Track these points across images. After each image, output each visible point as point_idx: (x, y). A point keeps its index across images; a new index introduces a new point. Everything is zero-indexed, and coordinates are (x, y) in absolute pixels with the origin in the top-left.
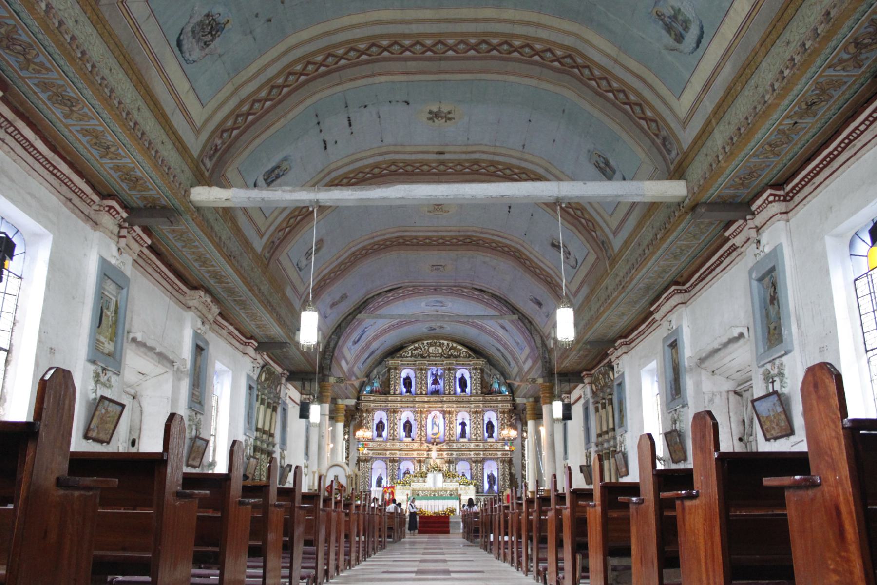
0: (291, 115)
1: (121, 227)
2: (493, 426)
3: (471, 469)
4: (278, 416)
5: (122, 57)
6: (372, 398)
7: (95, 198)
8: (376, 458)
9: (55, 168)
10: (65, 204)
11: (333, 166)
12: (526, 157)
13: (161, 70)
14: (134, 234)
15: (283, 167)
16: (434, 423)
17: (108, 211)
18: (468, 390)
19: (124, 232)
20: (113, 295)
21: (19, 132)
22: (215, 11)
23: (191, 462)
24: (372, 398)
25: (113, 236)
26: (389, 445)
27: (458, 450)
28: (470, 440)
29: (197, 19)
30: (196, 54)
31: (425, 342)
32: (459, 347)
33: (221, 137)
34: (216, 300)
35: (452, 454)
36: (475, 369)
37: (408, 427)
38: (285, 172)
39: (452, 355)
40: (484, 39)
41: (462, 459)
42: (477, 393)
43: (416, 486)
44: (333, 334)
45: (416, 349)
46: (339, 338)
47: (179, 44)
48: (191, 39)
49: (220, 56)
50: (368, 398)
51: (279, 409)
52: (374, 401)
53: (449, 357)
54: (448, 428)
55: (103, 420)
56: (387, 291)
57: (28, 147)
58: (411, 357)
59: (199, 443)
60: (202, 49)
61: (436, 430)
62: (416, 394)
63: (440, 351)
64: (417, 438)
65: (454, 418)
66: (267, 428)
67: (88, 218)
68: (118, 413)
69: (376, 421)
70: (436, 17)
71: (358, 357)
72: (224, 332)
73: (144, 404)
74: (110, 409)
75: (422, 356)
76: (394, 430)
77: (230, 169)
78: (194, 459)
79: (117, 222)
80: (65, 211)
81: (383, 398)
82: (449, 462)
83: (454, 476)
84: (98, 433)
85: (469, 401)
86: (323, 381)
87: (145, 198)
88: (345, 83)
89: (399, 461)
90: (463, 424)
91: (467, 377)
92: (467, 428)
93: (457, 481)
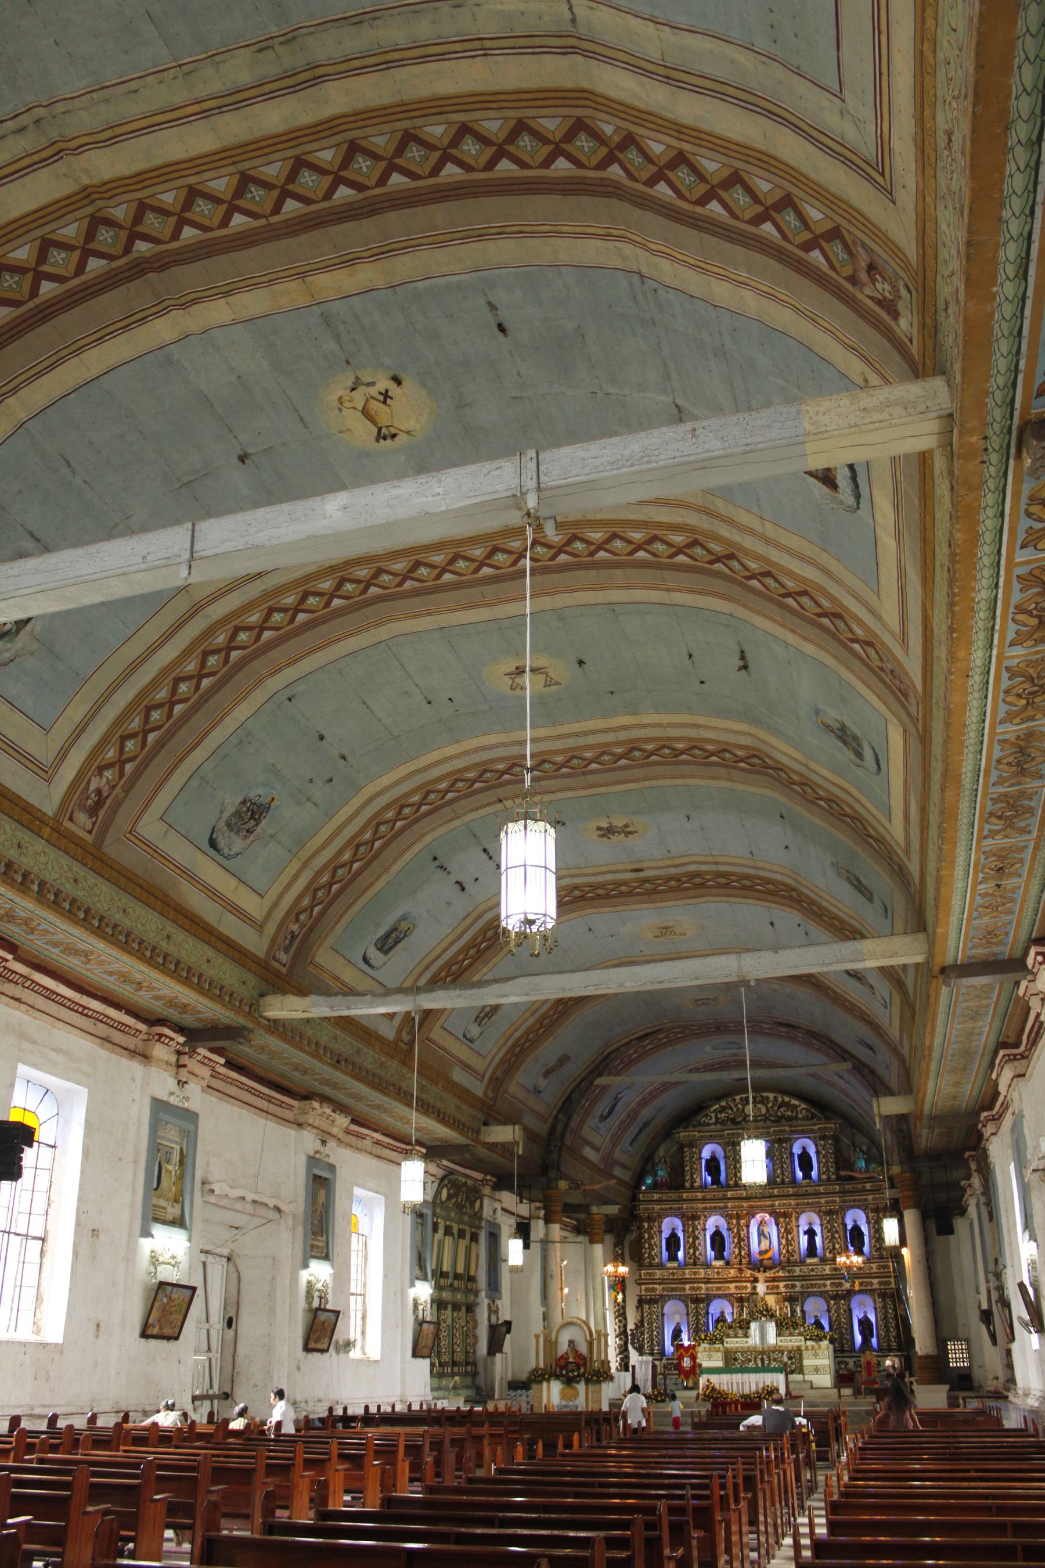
0: (395, 869)
1: (179, 1053)
2: (862, 1234)
3: (829, 1311)
4: (482, 1248)
5: (138, 889)
6: (656, 1196)
7: (142, 1027)
8: (670, 1298)
9: (85, 1008)
10: (102, 1046)
11: (482, 908)
12: (758, 864)
13: (193, 878)
14: (199, 1058)
15: (404, 926)
16: (761, 1234)
17: (158, 1040)
18: (814, 1174)
19: (185, 1059)
20: (176, 1143)
21: (38, 984)
22: (252, 794)
23: (312, 1345)
24: (656, 1196)
25: (169, 1068)
26: (688, 1273)
27: (802, 1278)
28: (823, 1260)
29: (230, 810)
30: (239, 844)
31: (738, 1098)
32: (795, 1102)
33: (297, 920)
34: (340, 1107)
35: (793, 1286)
36: (823, 1138)
37: (718, 1240)
38: (407, 933)
39: (783, 1116)
40: (631, 748)
41: (814, 1294)
42: (829, 1179)
43: (731, 1343)
44: (559, 1112)
45: (723, 1109)
46: (569, 1118)
47: (213, 844)
48: (227, 833)
49: (271, 836)
50: (648, 1197)
51: (483, 1237)
52: (660, 1201)
53: (779, 1120)
54: (784, 1241)
55: (165, 1311)
56: (639, 1039)
57: (50, 995)
58: (716, 1123)
59: (323, 1316)
60: (246, 837)
61: (765, 1244)
62: (728, 1186)
63: (764, 1111)
64: (735, 1261)
65: (794, 1224)
66: (460, 1269)
67: (133, 1053)
68: (187, 1299)
69: (666, 1234)
70: (555, 733)
71: (616, 1140)
72: (367, 1143)
73: (242, 1267)
74: (174, 1296)
75: (733, 1121)
76: (696, 1249)
77: (320, 952)
78: (317, 1341)
79: (172, 1049)
80: (103, 1053)
81: (674, 1195)
82: (791, 1299)
83: (795, 1325)
84: (161, 1328)
85: (817, 1194)
86: (548, 1187)
87: (201, 1020)
88: (463, 815)
89: (708, 1299)
90: (811, 1233)
91: (812, 1151)
92: (818, 1239)
93: (800, 1334)
